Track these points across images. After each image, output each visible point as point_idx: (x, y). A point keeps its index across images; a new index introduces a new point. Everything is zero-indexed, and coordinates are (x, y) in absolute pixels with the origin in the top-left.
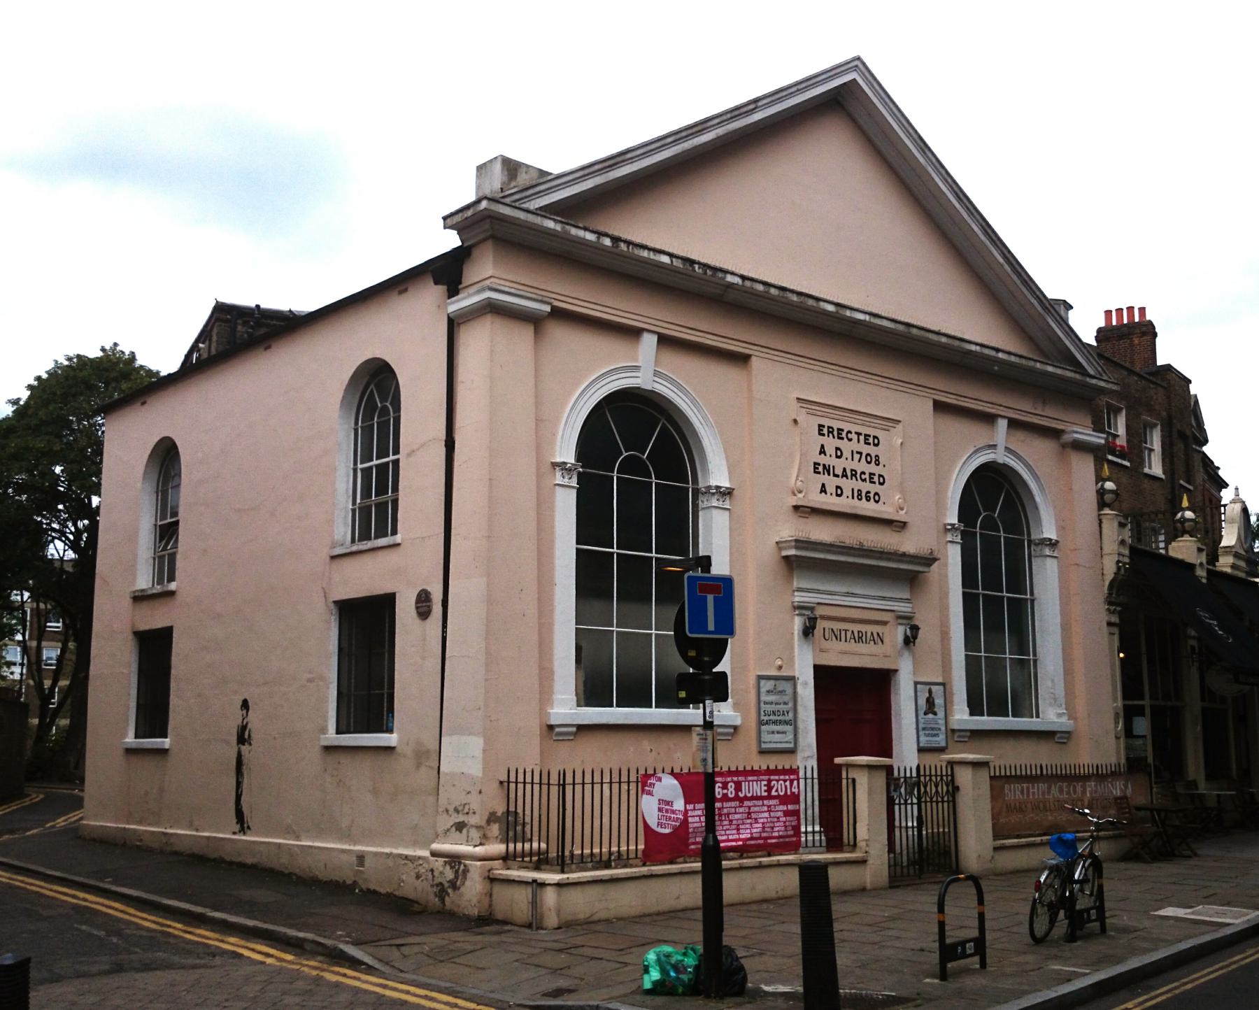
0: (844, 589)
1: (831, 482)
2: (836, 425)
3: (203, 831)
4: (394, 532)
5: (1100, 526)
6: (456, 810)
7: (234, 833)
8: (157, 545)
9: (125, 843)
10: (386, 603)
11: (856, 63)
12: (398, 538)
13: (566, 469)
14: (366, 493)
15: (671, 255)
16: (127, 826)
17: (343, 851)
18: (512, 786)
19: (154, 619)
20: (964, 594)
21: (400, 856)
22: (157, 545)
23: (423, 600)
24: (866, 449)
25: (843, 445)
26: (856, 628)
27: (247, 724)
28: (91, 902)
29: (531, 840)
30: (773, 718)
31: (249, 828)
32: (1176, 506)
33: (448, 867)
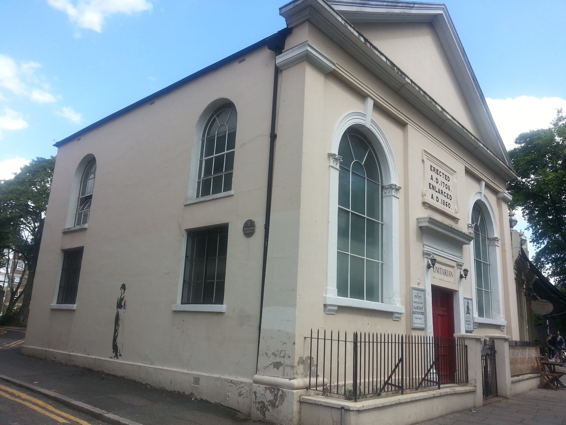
0: (440, 249)
2: (437, 167)
3: (92, 355)
5: (511, 235)
6: (274, 355)
7: (111, 358)
8: (79, 208)
9: (46, 358)
11: (443, 7)
12: (232, 192)
13: (335, 159)
14: (207, 172)
15: (386, 58)
16: (48, 349)
17: (184, 373)
18: (315, 341)
19: (72, 243)
21: (226, 380)
22: (79, 208)
25: (438, 177)
27: (124, 297)
28: (24, 400)
29: (317, 376)
30: (418, 310)
31: (120, 355)
33: (268, 392)
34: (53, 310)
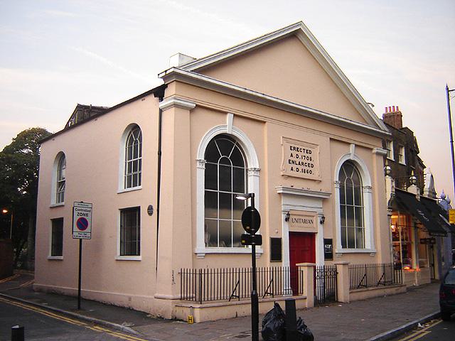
1: (295, 167)
2: (296, 146)
4: (140, 185)
10: (61, 220)
14: (130, 171)
19: (57, 215)
20: (341, 206)
23: (150, 209)
25: (299, 153)
26: (303, 218)
32: (409, 174)
34: (50, 260)
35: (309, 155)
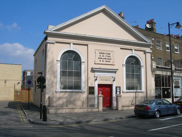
1: (101, 60)
2: (102, 52)
19: (105, 79)
24: (108, 55)
26: (105, 79)
35: (109, 55)
